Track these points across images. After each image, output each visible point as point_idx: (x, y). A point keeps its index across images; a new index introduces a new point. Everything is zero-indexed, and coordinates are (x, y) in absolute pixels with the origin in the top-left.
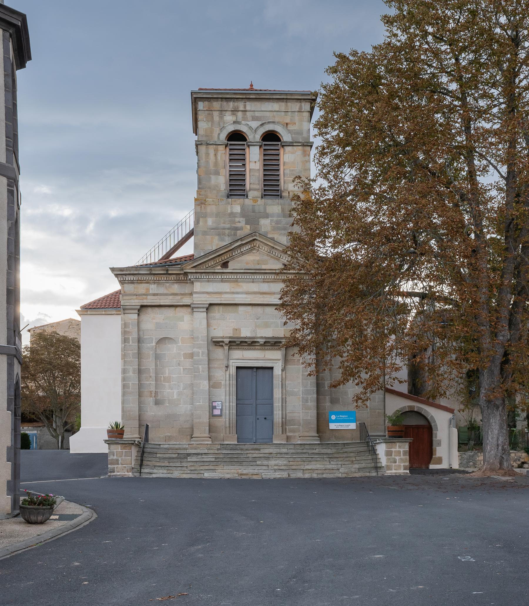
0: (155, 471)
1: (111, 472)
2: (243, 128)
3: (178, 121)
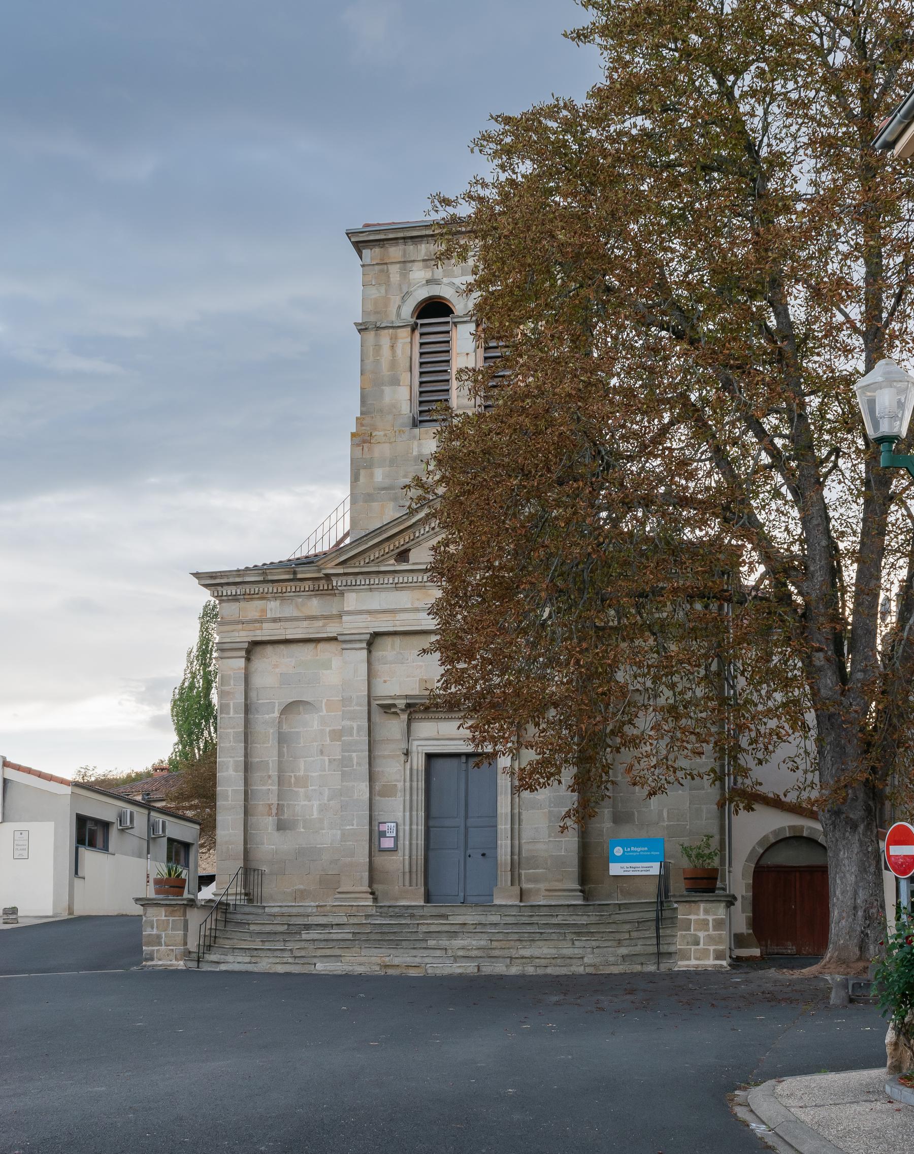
0: (230, 958)
1: (147, 960)
2: (446, 292)
3: (341, 288)
